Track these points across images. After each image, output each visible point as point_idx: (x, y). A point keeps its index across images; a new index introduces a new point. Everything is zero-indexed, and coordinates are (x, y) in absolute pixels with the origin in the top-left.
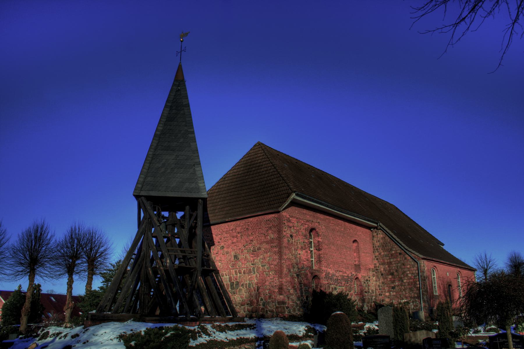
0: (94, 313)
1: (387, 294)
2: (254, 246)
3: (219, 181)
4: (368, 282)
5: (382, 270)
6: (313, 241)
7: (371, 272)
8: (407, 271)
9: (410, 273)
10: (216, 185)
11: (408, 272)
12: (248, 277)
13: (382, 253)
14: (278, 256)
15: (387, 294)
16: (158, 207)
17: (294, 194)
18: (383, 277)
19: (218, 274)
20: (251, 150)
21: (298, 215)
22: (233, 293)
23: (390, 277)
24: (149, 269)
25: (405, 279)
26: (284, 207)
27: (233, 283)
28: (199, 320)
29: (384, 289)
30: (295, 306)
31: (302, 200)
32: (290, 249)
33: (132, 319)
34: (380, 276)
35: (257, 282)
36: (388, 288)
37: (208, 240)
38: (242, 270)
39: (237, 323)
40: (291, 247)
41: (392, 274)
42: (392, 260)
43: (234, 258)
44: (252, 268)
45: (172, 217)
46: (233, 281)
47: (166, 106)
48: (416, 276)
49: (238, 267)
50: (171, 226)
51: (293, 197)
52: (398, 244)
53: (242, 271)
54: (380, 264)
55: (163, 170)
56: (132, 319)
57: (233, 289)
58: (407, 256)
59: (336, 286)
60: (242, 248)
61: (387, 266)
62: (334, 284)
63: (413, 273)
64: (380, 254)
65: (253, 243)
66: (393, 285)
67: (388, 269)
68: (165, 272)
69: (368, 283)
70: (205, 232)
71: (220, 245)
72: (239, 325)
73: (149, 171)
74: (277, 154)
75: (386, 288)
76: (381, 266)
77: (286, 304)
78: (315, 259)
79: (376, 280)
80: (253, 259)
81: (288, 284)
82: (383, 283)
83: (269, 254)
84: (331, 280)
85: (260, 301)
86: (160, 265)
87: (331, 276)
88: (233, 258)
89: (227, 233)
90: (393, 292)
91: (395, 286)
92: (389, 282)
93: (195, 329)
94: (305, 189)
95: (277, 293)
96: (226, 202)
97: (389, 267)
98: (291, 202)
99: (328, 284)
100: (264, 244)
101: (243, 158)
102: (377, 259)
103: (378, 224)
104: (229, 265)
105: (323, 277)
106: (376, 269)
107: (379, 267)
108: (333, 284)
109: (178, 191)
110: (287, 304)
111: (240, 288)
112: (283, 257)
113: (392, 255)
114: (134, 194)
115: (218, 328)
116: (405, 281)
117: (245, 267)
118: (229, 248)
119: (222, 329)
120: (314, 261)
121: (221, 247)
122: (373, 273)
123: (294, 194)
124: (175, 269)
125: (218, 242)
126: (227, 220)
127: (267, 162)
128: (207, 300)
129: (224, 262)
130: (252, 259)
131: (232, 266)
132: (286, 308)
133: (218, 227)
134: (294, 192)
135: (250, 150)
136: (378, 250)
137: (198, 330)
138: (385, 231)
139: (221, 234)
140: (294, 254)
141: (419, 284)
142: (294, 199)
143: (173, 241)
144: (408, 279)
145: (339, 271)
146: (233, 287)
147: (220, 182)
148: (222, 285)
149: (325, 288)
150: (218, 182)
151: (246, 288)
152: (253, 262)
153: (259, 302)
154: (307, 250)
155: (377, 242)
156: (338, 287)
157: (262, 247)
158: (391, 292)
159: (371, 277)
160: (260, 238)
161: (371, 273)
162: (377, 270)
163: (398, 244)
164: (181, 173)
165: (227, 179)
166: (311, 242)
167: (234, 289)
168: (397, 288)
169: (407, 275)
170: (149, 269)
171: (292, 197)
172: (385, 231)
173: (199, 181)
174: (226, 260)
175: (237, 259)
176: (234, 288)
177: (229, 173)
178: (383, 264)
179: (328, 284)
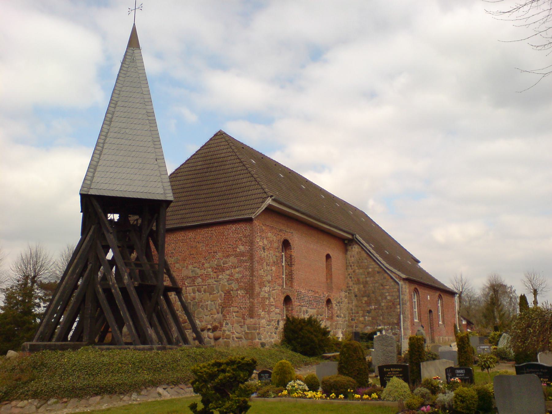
1: (361, 319)
2: (218, 259)
4: (340, 304)
5: (356, 290)
7: (343, 293)
8: (386, 293)
9: (389, 295)
11: (387, 294)
12: (210, 296)
13: (357, 271)
14: (249, 272)
15: (361, 319)
18: (357, 299)
20: (211, 139)
23: (366, 299)
24: (99, 286)
25: (383, 302)
29: (358, 313)
31: (274, 205)
34: (353, 297)
35: (221, 302)
36: (362, 312)
38: (202, 287)
41: (368, 296)
42: (368, 279)
44: (215, 286)
48: (397, 299)
49: (196, 284)
52: (377, 261)
53: (202, 289)
54: (354, 284)
58: (386, 275)
59: (308, 308)
60: (202, 261)
61: (362, 286)
63: (392, 296)
64: (354, 272)
65: (217, 256)
66: (368, 309)
67: (363, 289)
68: (120, 291)
69: (339, 306)
71: (173, 256)
75: (360, 312)
76: (355, 286)
78: (286, 275)
79: (348, 302)
80: (217, 275)
82: (356, 306)
83: (237, 269)
85: (224, 325)
90: (368, 316)
91: (371, 309)
92: (364, 305)
95: (246, 316)
97: (364, 287)
99: (300, 306)
100: (231, 258)
102: (351, 278)
103: (354, 236)
104: (185, 281)
106: (348, 289)
107: (352, 287)
111: (198, 309)
113: (368, 273)
116: (383, 304)
117: (207, 284)
118: (186, 260)
120: (285, 278)
122: (346, 294)
123: (271, 199)
127: (233, 158)
130: (215, 275)
132: (257, 334)
135: (209, 139)
136: (353, 267)
138: (361, 245)
139: (175, 242)
141: (400, 308)
142: (270, 205)
144: (386, 302)
145: (311, 291)
149: (297, 311)
151: (207, 309)
152: (217, 278)
153: (223, 326)
155: (351, 257)
156: (309, 310)
157: (229, 261)
158: (367, 317)
159: (344, 299)
160: (227, 250)
161: (343, 294)
162: (350, 290)
163: (377, 261)
165: (180, 174)
166: (283, 255)
168: (373, 313)
169: (386, 298)
170: (99, 286)
172: (361, 245)
178: (358, 282)
179: (300, 306)
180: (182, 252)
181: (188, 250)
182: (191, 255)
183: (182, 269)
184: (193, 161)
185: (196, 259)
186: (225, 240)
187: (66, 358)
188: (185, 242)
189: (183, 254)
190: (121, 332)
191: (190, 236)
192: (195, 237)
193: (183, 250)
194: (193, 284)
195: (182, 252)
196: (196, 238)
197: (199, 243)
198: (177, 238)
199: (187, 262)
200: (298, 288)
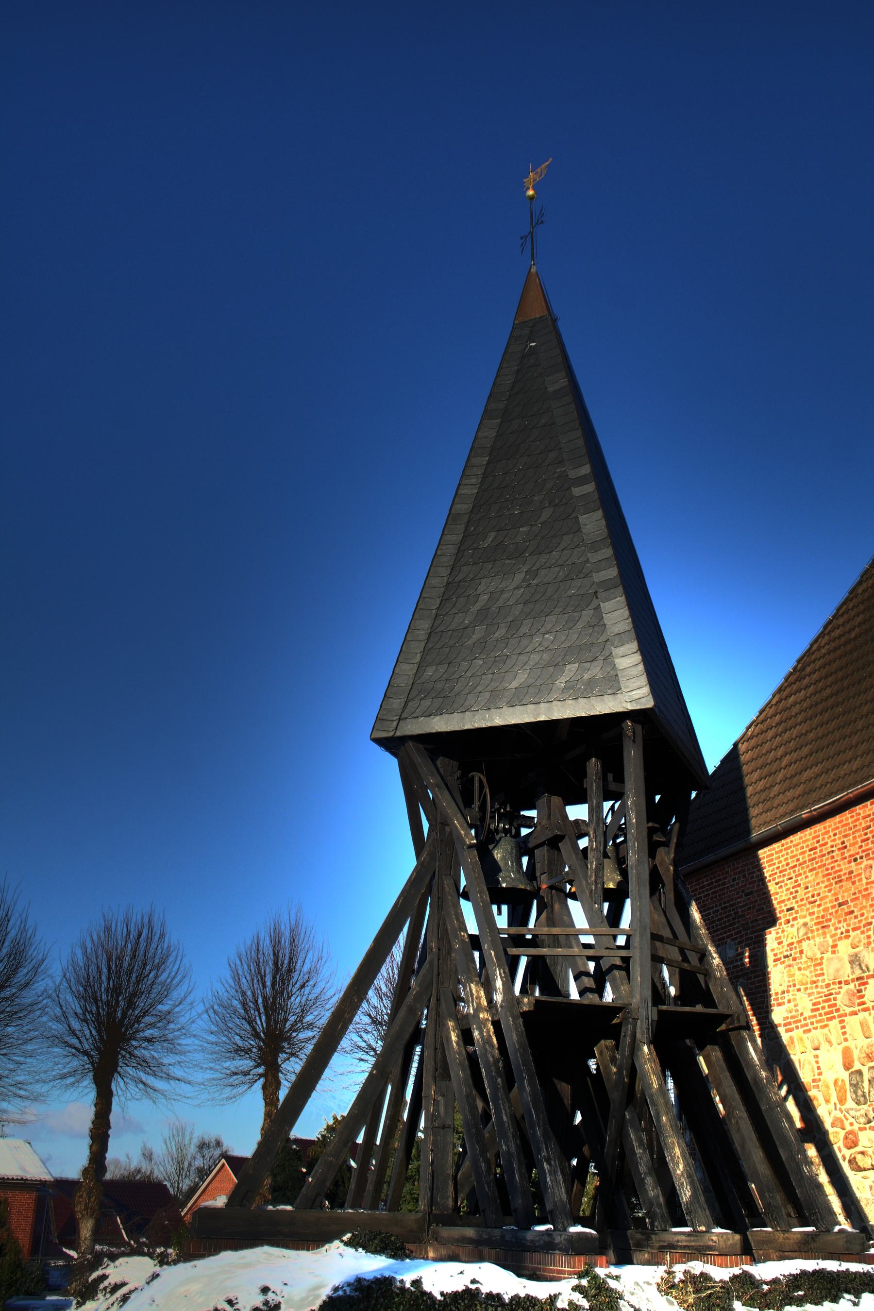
3: (782, 685)
10: (774, 702)
16: (480, 778)
19: (745, 1034)
22: (862, 1120)
27: (860, 1072)
28: (648, 1246)
33: (347, 1237)
37: (749, 908)
39: (811, 1265)
43: (852, 968)
45: (549, 815)
46: (857, 1066)
47: (487, 414)
50: (545, 847)
55: (479, 631)
56: (347, 1237)
57: (862, 1099)
70: (739, 878)
72: (820, 1274)
73: (430, 645)
86: (479, 1004)
88: (849, 965)
89: (814, 869)
93: (553, 1299)
96: (805, 750)
101: (860, 583)
109: (536, 700)
114: (375, 736)
115: (690, 1289)
119: (710, 1296)
121: (798, 929)
124: (524, 1014)
125: (788, 910)
126: (805, 814)
128: (677, 1151)
129: (817, 987)
131: (847, 1003)
133: (781, 851)
137: (571, 1303)
143: (557, 906)
146: (860, 1093)
147: (786, 688)
148: (762, 1079)
150: (780, 690)
164: (547, 633)
165: (808, 669)
167: (865, 1103)
173: (618, 649)
174: (824, 980)
175: (864, 972)
176: (864, 1096)
177: (815, 647)
180: (815, 901)
181: (830, 891)
182: (840, 905)
183: (822, 958)
184: (841, 620)
185: (856, 917)
186: (859, 814)
187: (466, 1296)
188: (820, 867)
189: (819, 906)
190: (429, 1227)
191: (830, 844)
192: (843, 843)
193: (819, 894)
194: (859, 1005)
195: (815, 901)
196: (846, 847)
197: (855, 860)
198: (798, 860)
199: (833, 932)
200: (801, 921)
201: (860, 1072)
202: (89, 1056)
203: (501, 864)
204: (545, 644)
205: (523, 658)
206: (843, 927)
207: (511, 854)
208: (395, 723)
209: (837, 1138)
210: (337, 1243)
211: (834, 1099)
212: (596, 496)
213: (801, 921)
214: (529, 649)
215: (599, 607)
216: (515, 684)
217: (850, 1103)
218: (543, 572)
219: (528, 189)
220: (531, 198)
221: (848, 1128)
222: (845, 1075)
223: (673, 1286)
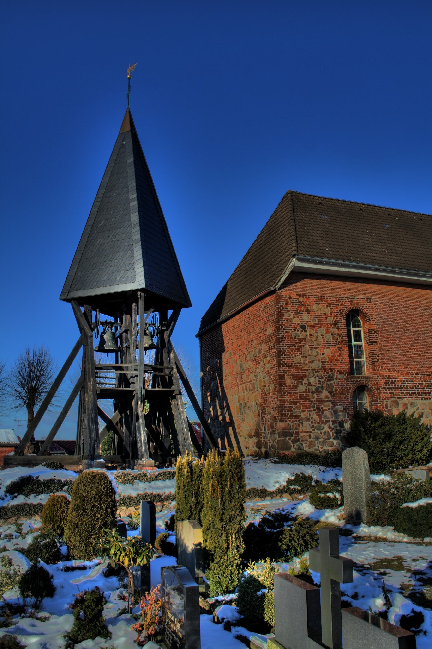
0: (12, 456)
6: (364, 330)
17: (294, 259)
21: (318, 291)
26: (280, 283)
30: (313, 438)
32: (301, 347)
40: (302, 344)
46: (241, 402)
51: (293, 265)
62: (409, 398)
74: (387, 214)
77: (292, 436)
81: (295, 404)
84: (401, 390)
87: (402, 383)
94: (330, 249)
98: (292, 273)
105: (381, 387)
108: (406, 398)
110: (294, 435)
112: (284, 362)
134: (294, 256)
140: (309, 355)
154: (341, 346)
171: (291, 265)
200: (230, 351)
201: (241, 404)
202: (23, 399)
203: (106, 340)
204: (115, 264)
205: (108, 269)
206: (239, 354)
207: (110, 337)
208: (67, 294)
209: (236, 425)
210: (41, 465)
211: (236, 413)
212: (137, 206)
213: (230, 351)
214: (110, 266)
215: (133, 250)
216: (105, 279)
217: (239, 415)
218: (117, 236)
219: (128, 74)
220: (129, 79)
221: (239, 423)
222: (238, 405)
223: (118, 477)
